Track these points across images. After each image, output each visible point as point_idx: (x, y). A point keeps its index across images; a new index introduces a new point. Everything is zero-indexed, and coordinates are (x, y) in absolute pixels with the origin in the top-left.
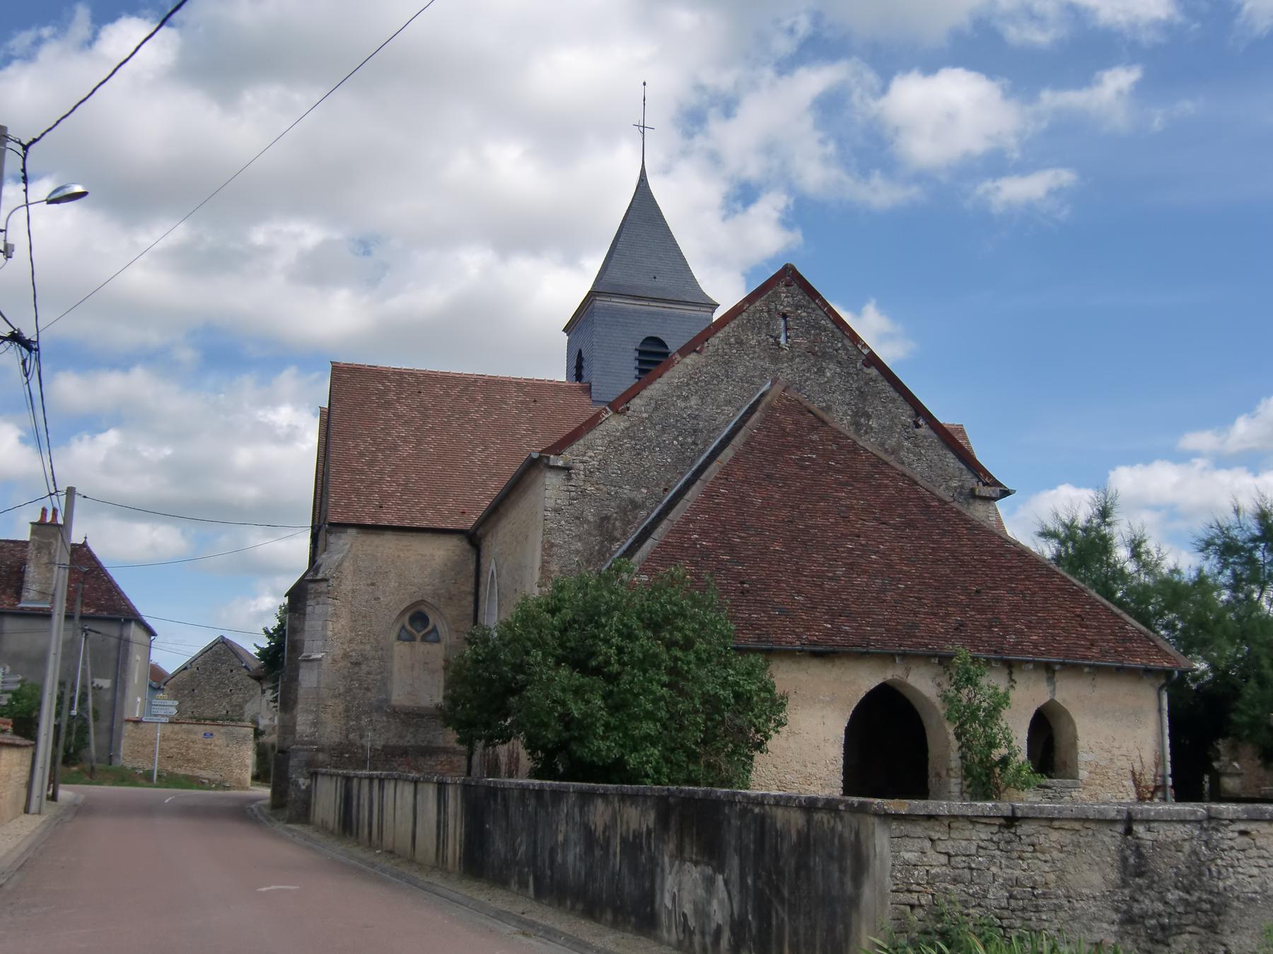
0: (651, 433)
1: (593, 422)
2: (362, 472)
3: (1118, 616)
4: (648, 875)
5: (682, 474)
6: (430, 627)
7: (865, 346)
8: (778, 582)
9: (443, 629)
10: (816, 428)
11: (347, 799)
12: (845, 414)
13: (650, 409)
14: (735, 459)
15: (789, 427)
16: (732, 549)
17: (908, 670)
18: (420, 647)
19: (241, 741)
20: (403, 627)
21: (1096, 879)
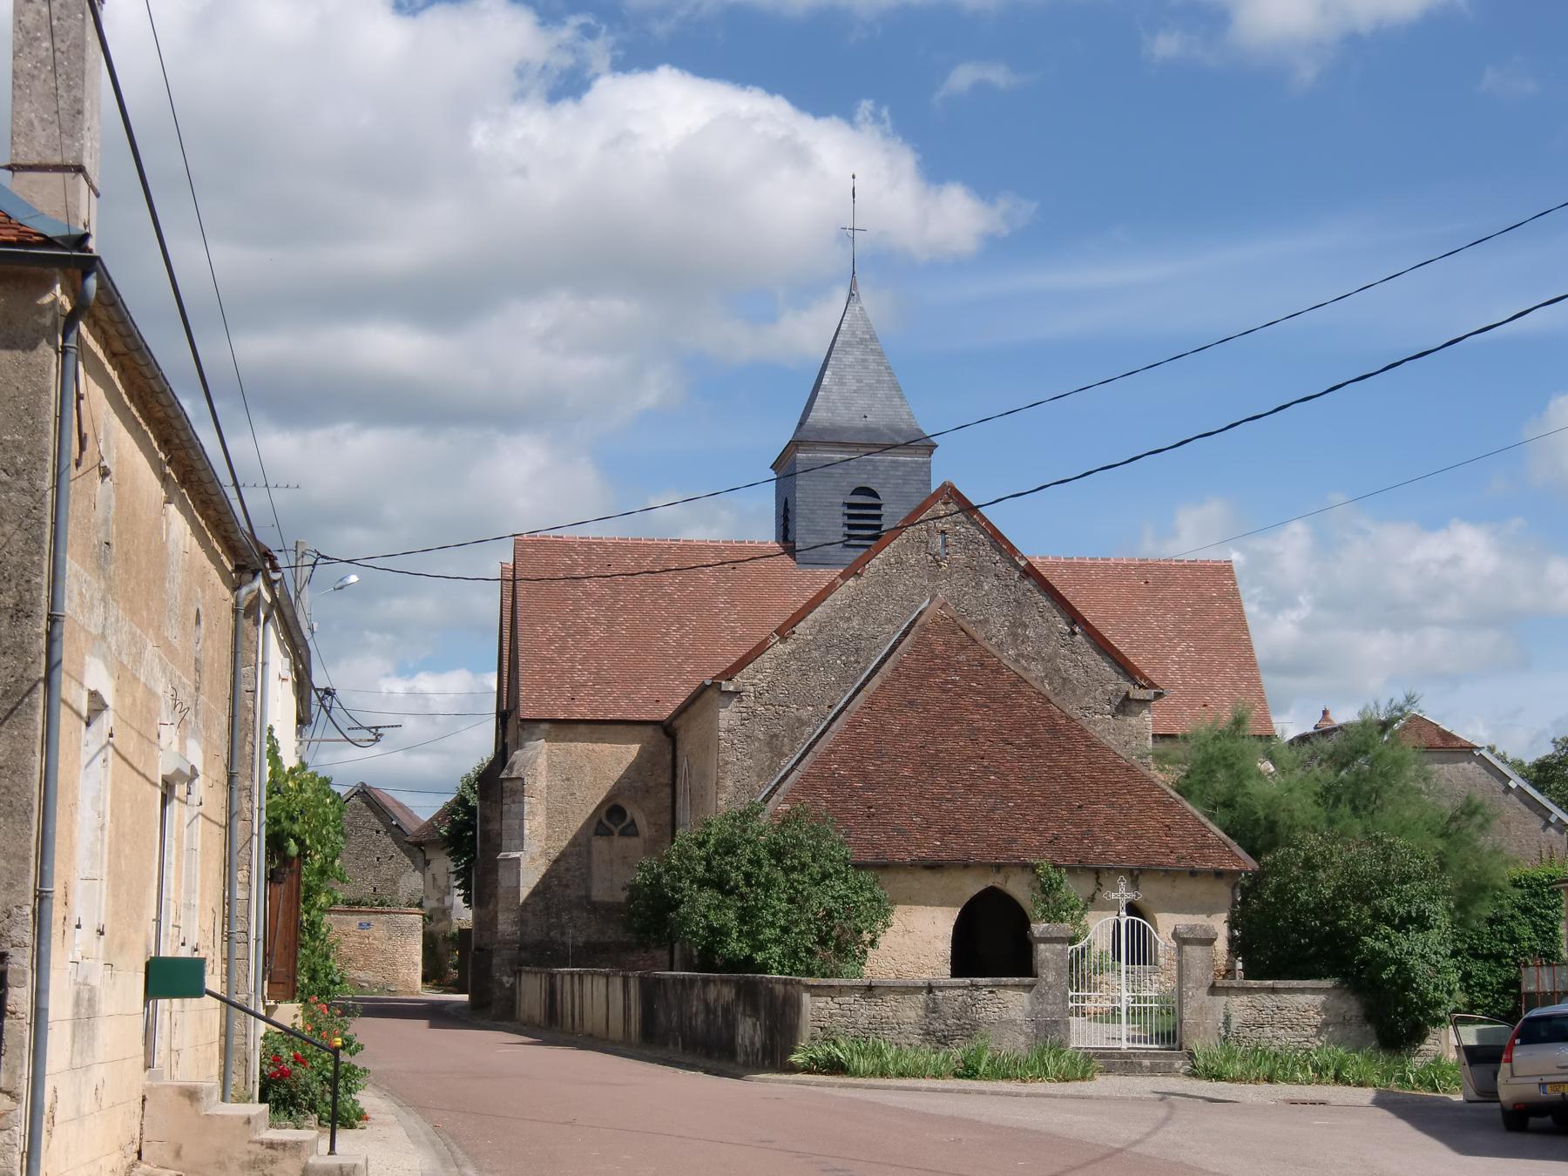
0: (815, 654)
1: (760, 649)
2: (552, 661)
3: (1203, 825)
4: (731, 1026)
5: (845, 692)
6: (628, 820)
7: (1022, 557)
8: (900, 805)
9: (642, 822)
10: (965, 648)
11: (552, 993)
12: (1003, 626)
13: (814, 631)
14: (882, 687)
15: (939, 649)
16: (865, 776)
17: (1007, 879)
18: (619, 842)
19: (403, 931)
20: (600, 822)
21: (912, 1014)
